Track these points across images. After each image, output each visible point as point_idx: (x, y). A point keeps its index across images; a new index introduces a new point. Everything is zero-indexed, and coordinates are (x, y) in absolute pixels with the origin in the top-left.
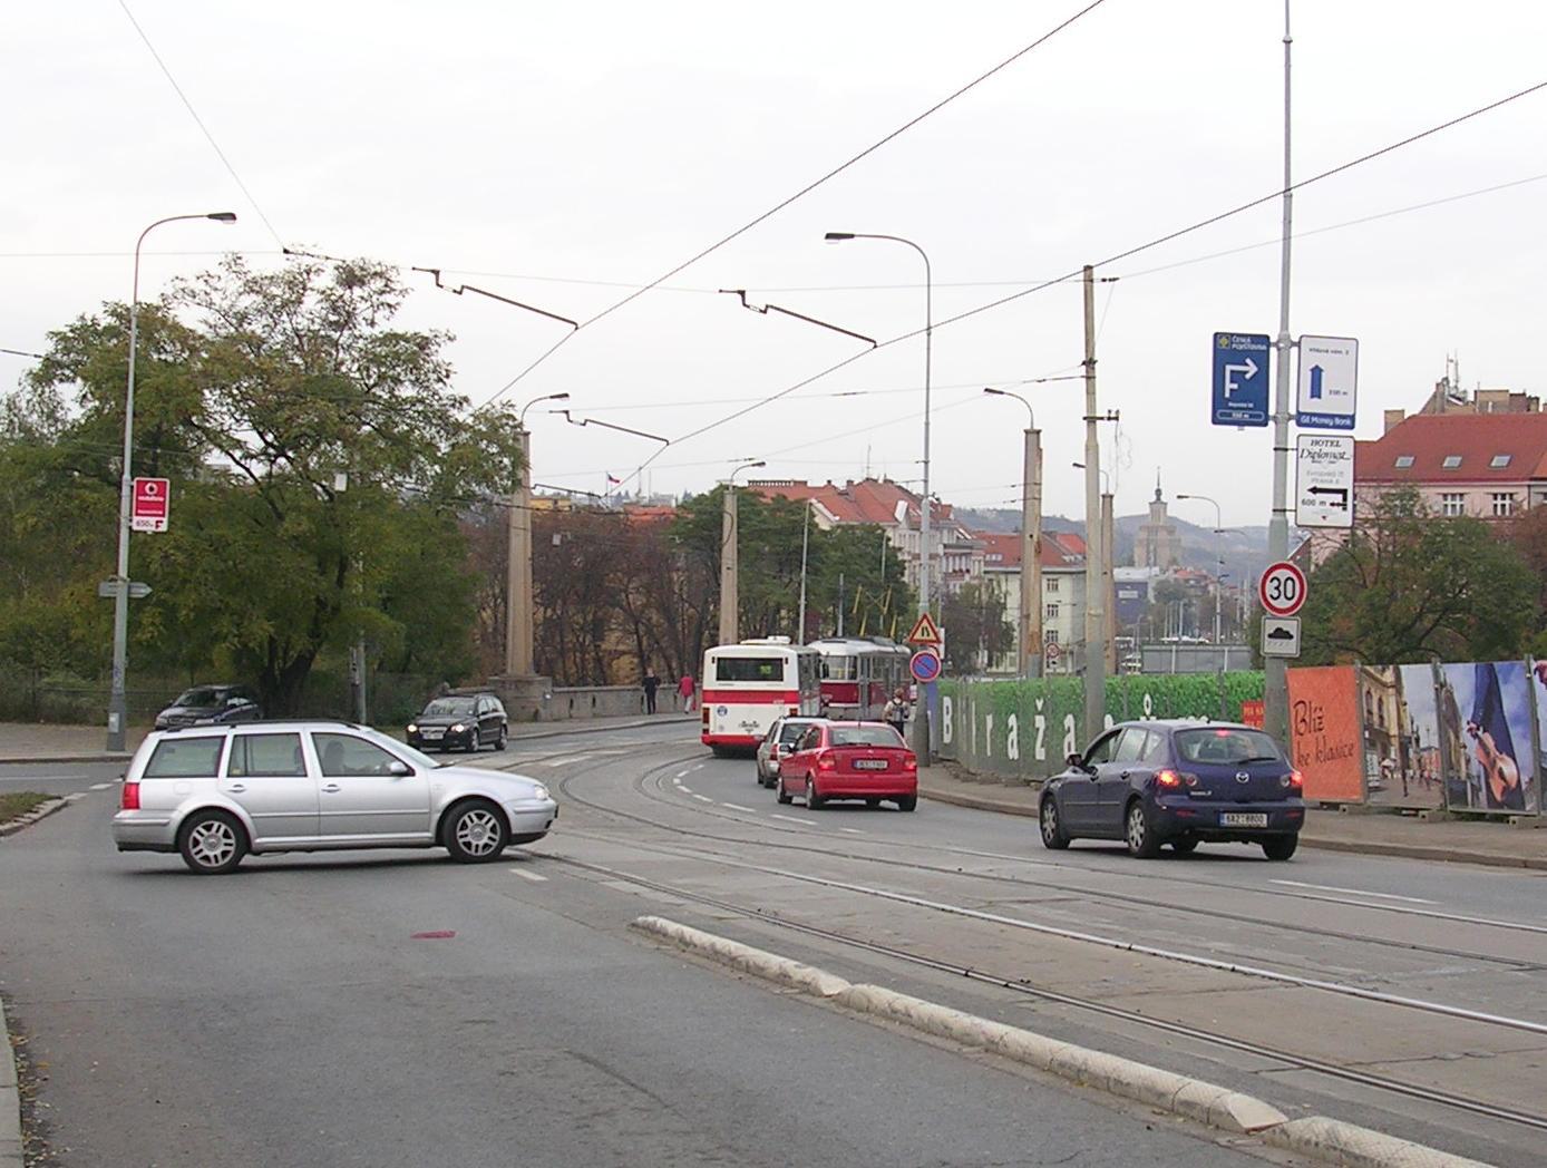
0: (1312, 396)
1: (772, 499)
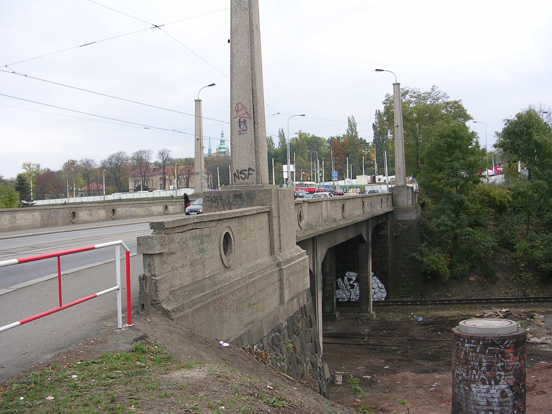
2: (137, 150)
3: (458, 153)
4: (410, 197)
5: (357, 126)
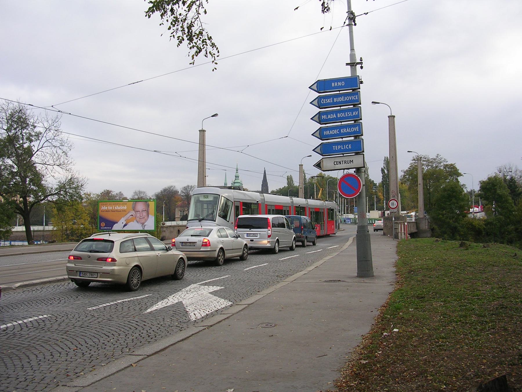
0: (346, 64)
1: (324, 118)
2: (185, 185)
3: (454, 200)
4: (427, 224)
5: (368, 170)
